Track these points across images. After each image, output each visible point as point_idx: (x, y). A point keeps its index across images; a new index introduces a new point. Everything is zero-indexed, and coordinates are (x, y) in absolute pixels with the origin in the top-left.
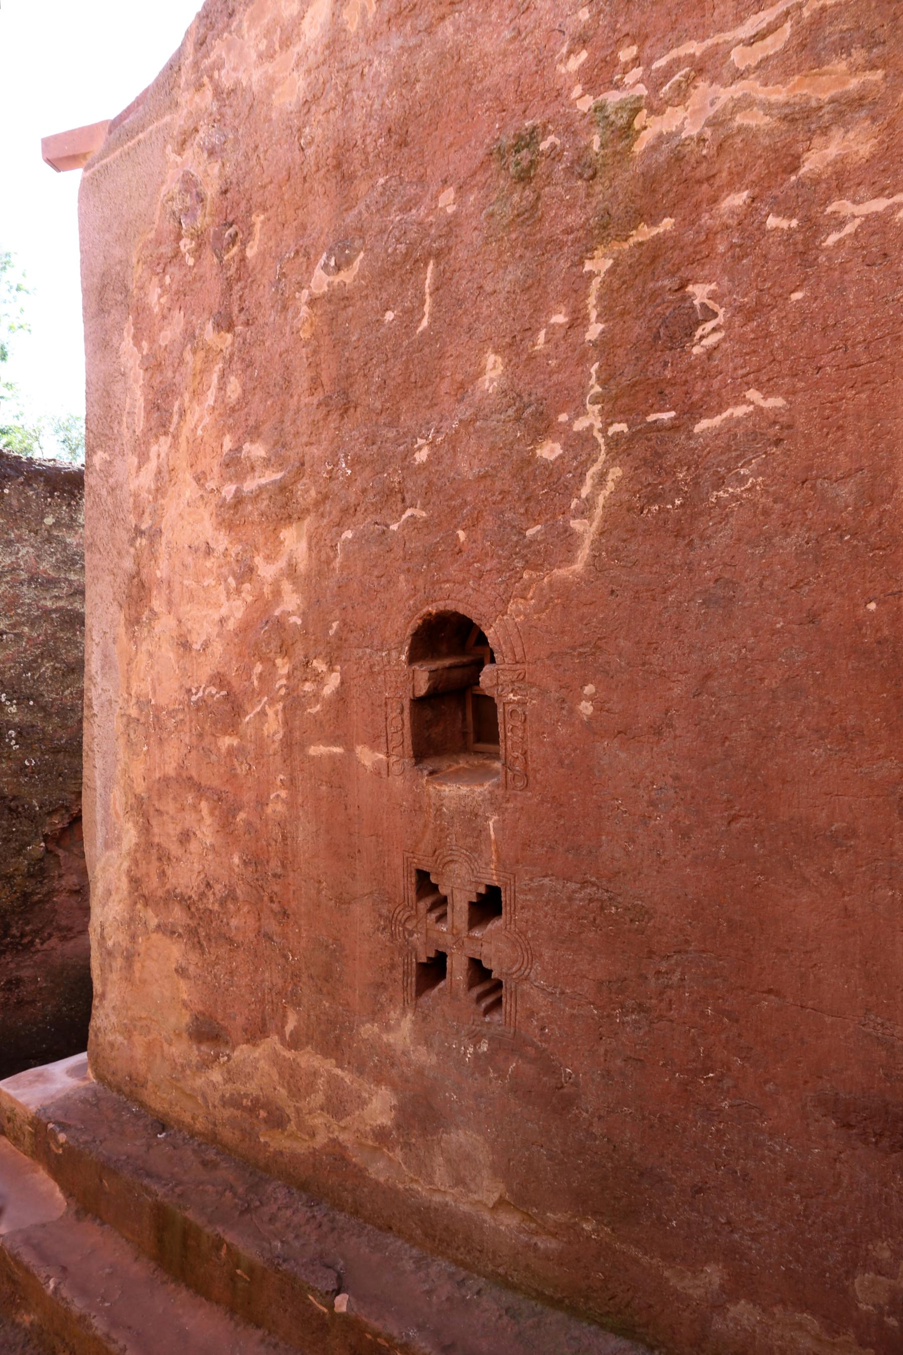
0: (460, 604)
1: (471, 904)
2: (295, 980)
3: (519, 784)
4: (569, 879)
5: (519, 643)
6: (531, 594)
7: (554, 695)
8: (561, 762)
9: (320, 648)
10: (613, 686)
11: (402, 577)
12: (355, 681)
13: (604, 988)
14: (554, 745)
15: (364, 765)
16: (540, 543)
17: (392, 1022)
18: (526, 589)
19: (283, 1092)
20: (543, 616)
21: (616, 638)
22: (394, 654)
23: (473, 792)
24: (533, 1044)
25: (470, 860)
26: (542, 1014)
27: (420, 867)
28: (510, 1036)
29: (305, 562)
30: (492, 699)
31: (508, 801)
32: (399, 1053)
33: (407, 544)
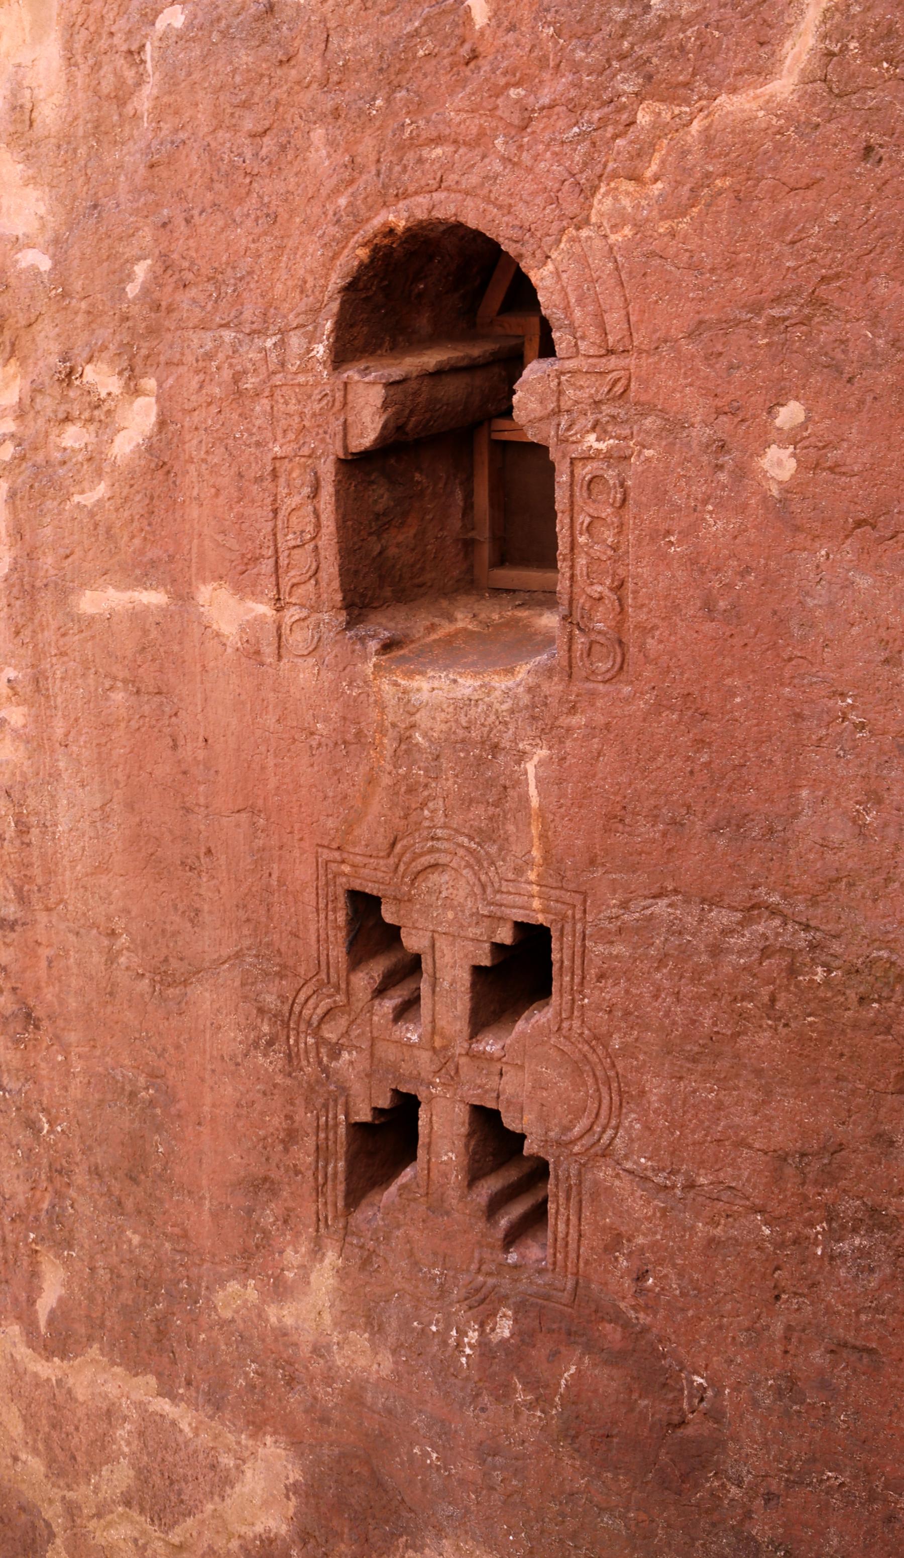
0: (469, 202)
1: (477, 970)
2: (59, 1181)
3: (602, 666)
4: (713, 901)
5: (618, 300)
6: (654, 167)
7: (700, 433)
8: (709, 606)
9: (103, 334)
10: (852, 404)
11: (318, 134)
12: (196, 417)
13: (789, 1171)
14: (694, 562)
15: (218, 635)
16: (687, 23)
17: (290, 1275)
18: (642, 153)
19: (35, 1465)
20: (684, 225)
21: (869, 275)
22: (296, 341)
23: (488, 689)
24: (617, 1317)
25: (477, 862)
26: (640, 1240)
27: (357, 885)
28: (566, 1297)
29: (57, 99)
30: (539, 450)
31: (573, 710)
32: (305, 1350)
33: (334, 41)
